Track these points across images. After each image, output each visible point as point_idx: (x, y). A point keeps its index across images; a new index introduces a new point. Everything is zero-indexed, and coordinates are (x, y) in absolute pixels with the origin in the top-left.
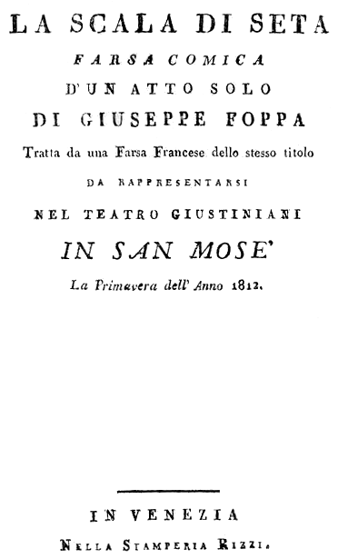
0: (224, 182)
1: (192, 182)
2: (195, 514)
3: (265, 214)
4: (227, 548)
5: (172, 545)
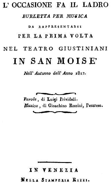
0: (73, 26)
1: (63, 27)
2: (64, 170)
3: (94, 48)
4: (76, 181)
5: (58, 180)
